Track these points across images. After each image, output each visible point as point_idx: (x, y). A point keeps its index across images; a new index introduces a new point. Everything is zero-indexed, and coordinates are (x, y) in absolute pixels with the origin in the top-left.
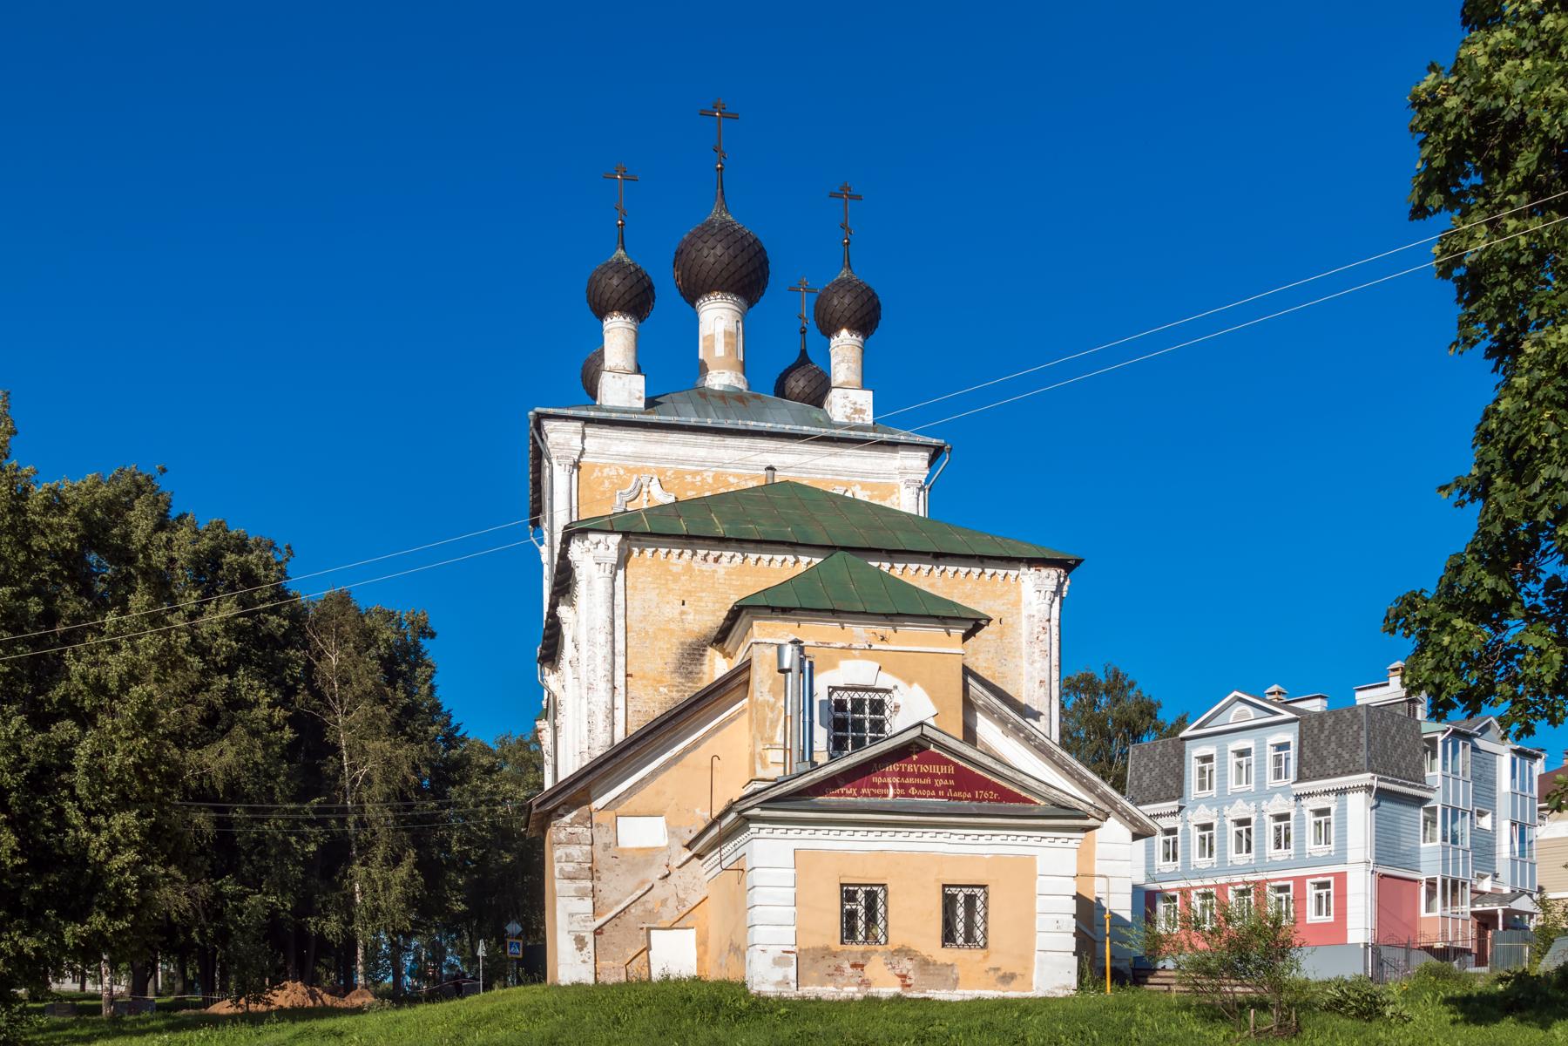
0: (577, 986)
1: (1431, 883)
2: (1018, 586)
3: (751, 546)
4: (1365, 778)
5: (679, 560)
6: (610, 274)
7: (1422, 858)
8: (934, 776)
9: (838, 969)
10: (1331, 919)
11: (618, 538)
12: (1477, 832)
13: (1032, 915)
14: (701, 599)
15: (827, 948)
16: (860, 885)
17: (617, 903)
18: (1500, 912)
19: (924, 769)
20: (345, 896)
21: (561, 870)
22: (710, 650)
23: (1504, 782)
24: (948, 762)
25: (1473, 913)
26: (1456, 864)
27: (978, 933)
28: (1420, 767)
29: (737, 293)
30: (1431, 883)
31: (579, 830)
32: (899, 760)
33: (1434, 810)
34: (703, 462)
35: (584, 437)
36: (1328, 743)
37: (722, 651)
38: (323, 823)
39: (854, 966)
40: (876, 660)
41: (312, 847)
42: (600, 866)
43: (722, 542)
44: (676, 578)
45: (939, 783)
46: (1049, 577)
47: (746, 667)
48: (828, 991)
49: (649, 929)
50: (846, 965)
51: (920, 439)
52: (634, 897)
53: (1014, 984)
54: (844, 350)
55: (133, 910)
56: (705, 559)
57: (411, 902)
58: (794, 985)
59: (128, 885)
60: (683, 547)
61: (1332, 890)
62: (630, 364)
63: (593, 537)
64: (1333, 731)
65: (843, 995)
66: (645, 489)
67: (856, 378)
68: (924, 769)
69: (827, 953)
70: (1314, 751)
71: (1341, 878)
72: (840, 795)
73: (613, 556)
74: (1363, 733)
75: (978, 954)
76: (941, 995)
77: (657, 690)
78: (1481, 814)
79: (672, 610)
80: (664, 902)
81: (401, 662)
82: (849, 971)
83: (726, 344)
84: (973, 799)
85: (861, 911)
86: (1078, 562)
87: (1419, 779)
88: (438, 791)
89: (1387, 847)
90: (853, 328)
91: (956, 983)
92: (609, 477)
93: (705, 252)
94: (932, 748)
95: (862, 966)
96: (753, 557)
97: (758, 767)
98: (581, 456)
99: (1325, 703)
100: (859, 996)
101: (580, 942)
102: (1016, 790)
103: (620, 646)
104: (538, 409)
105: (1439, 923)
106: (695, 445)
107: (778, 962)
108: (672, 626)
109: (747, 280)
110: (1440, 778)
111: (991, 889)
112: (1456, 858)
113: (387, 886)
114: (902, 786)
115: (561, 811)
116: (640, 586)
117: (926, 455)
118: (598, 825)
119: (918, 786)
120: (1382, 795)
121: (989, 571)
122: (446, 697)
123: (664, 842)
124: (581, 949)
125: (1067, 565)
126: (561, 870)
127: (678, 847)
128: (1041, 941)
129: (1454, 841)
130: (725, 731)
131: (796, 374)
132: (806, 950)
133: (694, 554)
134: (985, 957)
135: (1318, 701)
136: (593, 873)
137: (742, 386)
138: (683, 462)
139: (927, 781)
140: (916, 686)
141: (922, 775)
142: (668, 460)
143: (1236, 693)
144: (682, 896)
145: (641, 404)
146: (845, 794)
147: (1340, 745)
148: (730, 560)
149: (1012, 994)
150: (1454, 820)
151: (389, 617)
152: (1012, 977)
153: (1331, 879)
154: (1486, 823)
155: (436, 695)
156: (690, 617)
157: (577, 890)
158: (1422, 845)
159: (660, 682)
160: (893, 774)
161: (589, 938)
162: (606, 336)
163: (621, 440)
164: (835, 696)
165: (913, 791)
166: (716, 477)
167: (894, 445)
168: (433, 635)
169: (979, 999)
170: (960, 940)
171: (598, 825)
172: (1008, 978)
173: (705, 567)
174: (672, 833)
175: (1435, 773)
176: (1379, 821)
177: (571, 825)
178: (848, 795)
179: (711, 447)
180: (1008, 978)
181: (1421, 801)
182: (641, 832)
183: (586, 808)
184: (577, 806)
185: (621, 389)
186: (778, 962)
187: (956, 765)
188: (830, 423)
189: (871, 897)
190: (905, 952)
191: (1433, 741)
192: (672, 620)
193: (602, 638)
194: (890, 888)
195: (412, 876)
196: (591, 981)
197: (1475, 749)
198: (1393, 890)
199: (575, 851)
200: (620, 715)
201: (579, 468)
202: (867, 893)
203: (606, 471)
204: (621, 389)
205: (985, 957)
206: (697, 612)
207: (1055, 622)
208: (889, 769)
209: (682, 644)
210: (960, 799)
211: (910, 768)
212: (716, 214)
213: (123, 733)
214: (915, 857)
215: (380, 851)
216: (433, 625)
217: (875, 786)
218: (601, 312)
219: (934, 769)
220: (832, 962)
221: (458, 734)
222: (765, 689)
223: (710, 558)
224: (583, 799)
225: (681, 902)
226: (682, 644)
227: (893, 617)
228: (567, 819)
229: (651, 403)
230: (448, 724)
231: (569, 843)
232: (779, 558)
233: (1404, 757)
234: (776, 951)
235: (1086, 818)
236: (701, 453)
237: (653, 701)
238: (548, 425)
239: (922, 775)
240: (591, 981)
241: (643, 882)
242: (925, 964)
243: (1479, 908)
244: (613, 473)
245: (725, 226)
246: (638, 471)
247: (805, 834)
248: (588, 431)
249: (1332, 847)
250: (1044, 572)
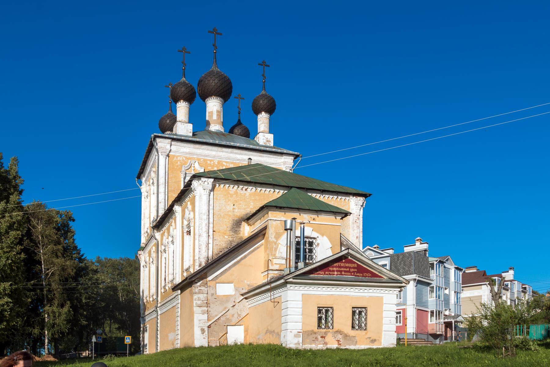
0: (202, 348)
1: (432, 312)
2: (349, 203)
3: (259, 185)
4: (414, 276)
5: (233, 189)
6: (181, 86)
7: (429, 304)
8: (350, 268)
9: (316, 338)
10: (401, 324)
11: (212, 180)
12: (445, 294)
13: (382, 318)
14: (240, 204)
15: (313, 331)
16: (324, 307)
17: (216, 316)
18: (453, 322)
19: (347, 265)
20: (41, 319)
21: (196, 303)
22: (243, 223)
23: (452, 279)
24: (355, 263)
25: (445, 323)
26: (439, 306)
27: (363, 325)
28: (429, 273)
29: (221, 97)
30: (432, 312)
31: (203, 288)
32: (338, 262)
33: (433, 287)
34: (214, 157)
35: (171, 145)
36: (400, 264)
37: (248, 223)
38: (34, 290)
39: (322, 337)
40: (311, 227)
41: (30, 300)
42: (210, 302)
43: (249, 183)
44: (231, 196)
45: (352, 270)
46: (361, 200)
47: (265, 228)
48: (314, 347)
49: (227, 325)
50: (319, 337)
51: (291, 152)
52: (222, 313)
53: (375, 343)
54: (263, 119)
55: (7, 321)
56: (242, 189)
57: (68, 321)
58: (301, 344)
59: (6, 311)
60: (235, 184)
61: (401, 315)
62: (187, 120)
63: (203, 179)
64: (402, 260)
65: (318, 348)
66: (193, 165)
67: (267, 130)
68: (347, 265)
69: (313, 332)
70: (396, 267)
71: (404, 310)
72: (318, 274)
73: (210, 187)
74: (413, 261)
75: (363, 332)
76: (352, 347)
77: (224, 237)
78: (446, 289)
79: (230, 207)
80: (233, 315)
81: (64, 229)
82: (320, 339)
83: (217, 115)
84: (363, 276)
85: (324, 316)
86: (370, 195)
87: (429, 276)
88: (75, 278)
89: (420, 300)
90: (266, 112)
91: (356, 343)
92: (179, 160)
93: (211, 82)
94: (349, 258)
95: (324, 337)
96: (259, 189)
97: (270, 265)
98: (169, 152)
99: (393, 251)
100: (325, 348)
101: (203, 331)
102: (377, 273)
103: (211, 220)
104: (155, 134)
105: (434, 325)
106: (211, 150)
107: (296, 336)
108: (230, 213)
109: (225, 93)
110: (435, 277)
111: (368, 309)
112: (439, 304)
113: (60, 314)
114: (339, 271)
115: (196, 281)
116: (218, 198)
117: (293, 158)
118: (209, 286)
119: (345, 271)
120: (419, 282)
121: (340, 197)
122: (79, 243)
123: (233, 293)
124: (203, 333)
125: (365, 196)
126: (196, 303)
127: (238, 295)
128: (385, 327)
129: (439, 298)
130: (256, 252)
131: (237, 128)
132: (305, 332)
133: (238, 187)
134: (366, 333)
135: (391, 250)
136: (208, 304)
137: (223, 130)
138: (207, 156)
139: (348, 269)
140: (325, 237)
141: (346, 267)
142: (202, 155)
143: (368, 247)
144: (239, 313)
145: (191, 134)
146: (320, 274)
147: (405, 265)
148: (251, 190)
149: (375, 347)
150: (439, 290)
151: (58, 213)
152: (375, 340)
153: (401, 311)
154: (447, 292)
155: (75, 242)
156: (236, 210)
157: (202, 311)
158: (429, 299)
159: (225, 234)
160: (336, 267)
161: (206, 329)
162: (178, 109)
163: (185, 147)
164: (297, 240)
165: (343, 273)
166: (219, 162)
167: (282, 154)
168: (74, 220)
169: (370, 349)
170: (357, 328)
171: (209, 286)
172: (373, 341)
173: (242, 192)
174: (236, 290)
175: (433, 274)
176: (417, 290)
177: (200, 286)
178: (321, 275)
179: (217, 151)
180: (373, 341)
181: (428, 284)
182: (225, 289)
183: (205, 280)
184: (202, 279)
185: (183, 128)
186: (296, 336)
187: (357, 264)
188: (258, 145)
189: (327, 311)
190: (339, 332)
191: (433, 264)
192: (230, 211)
193: (205, 217)
194: (334, 309)
195: (69, 311)
196: (207, 345)
197: (445, 267)
198: (421, 314)
199: (202, 296)
200: (211, 246)
201: (169, 157)
202: (326, 310)
203: (179, 158)
204: (183, 128)
205: (366, 333)
206: (238, 208)
207: (361, 216)
208: (335, 265)
209: (233, 220)
210: (359, 276)
211: (342, 265)
212: (214, 68)
213: (5, 250)
214: (343, 296)
215: (56, 302)
216: (74, 216)
217: (330, 271)
218: (176, 101)
219: (350, 265)
220: (314, 336)
221: (83, 258)
222: (273, 237)
223: (244, 189)
224: (204, 277)
225: (239, 315)
226: (233, 220)
227: (318, 211)
228: (199, 284)
229: (194, 135)
230: (79, 254)
231: (199, 293)
232: (268, 190)
233: (424, 269)
234: (295, 332)
235: (402, 283)
236: (214, 153)
237: (223, 242)
238: (158, 140)
239: (346, 267)
240: (207, 345)
241: (225, 308)
242: (346, 336)
243: (446, 320)
244: (181, 159)
245: (218, 73)
246: (190, 158)
247: (306, 288)
248: (173, 143)
249: (402, 300)
250: (359, 198)
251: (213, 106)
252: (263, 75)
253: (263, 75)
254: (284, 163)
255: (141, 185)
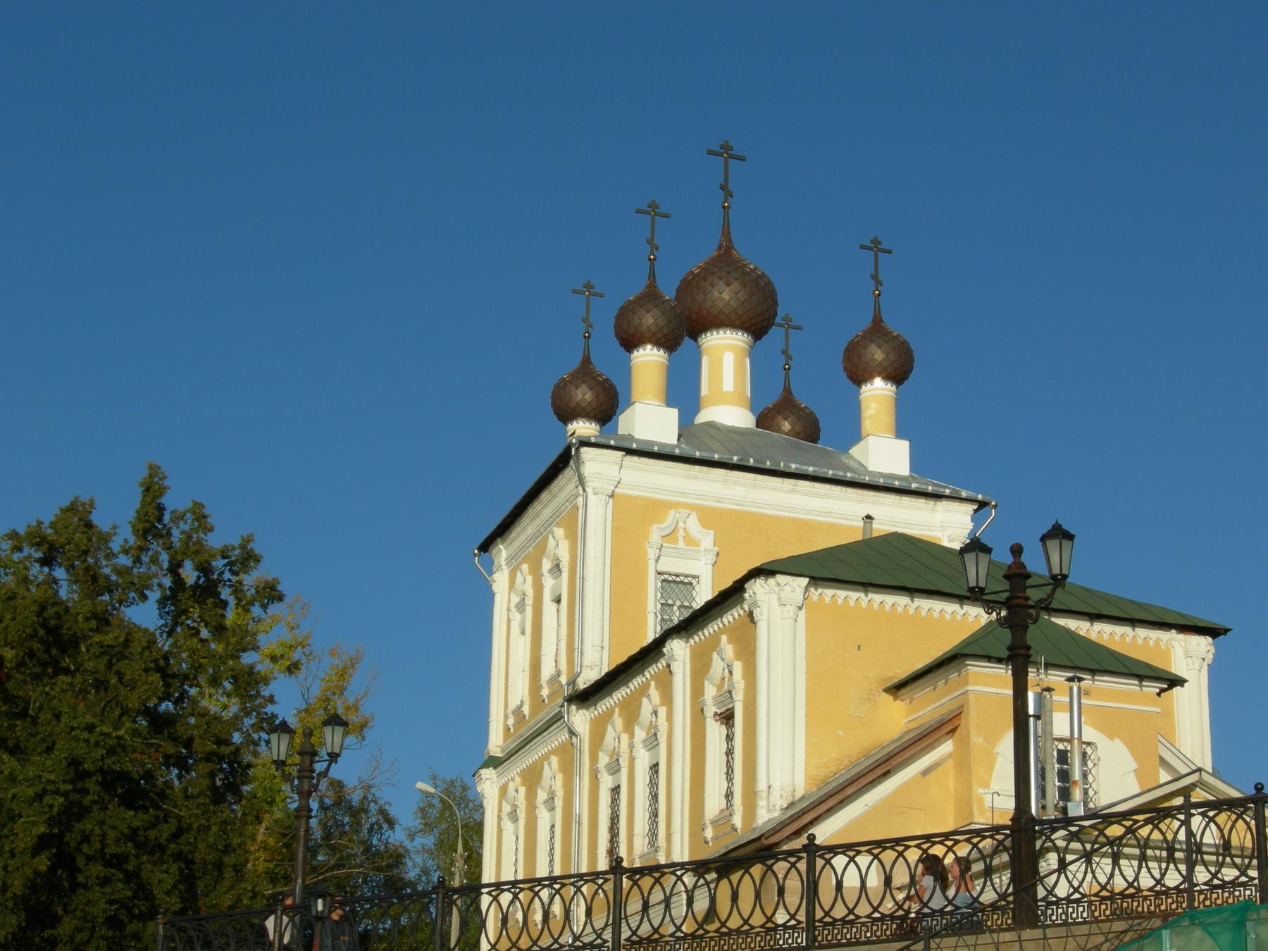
46: (1202, 645)
66: (681, 524)
86: (1226, 631)
167: (937, 496)
185: (650, 419)
246: (677, 505)
251: (725, 354)
252: (875, 277)
253: (875, 277)
254: (947, 524)
255: (491, 573)
